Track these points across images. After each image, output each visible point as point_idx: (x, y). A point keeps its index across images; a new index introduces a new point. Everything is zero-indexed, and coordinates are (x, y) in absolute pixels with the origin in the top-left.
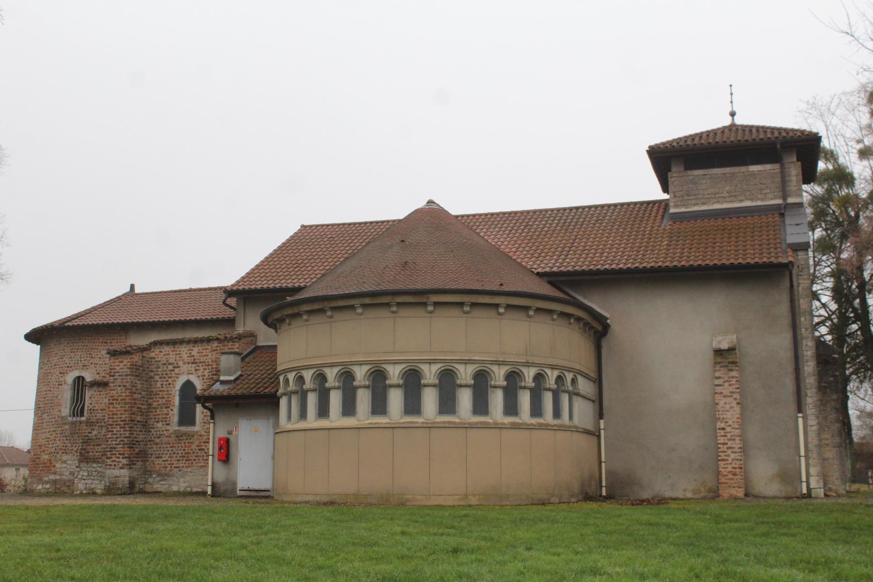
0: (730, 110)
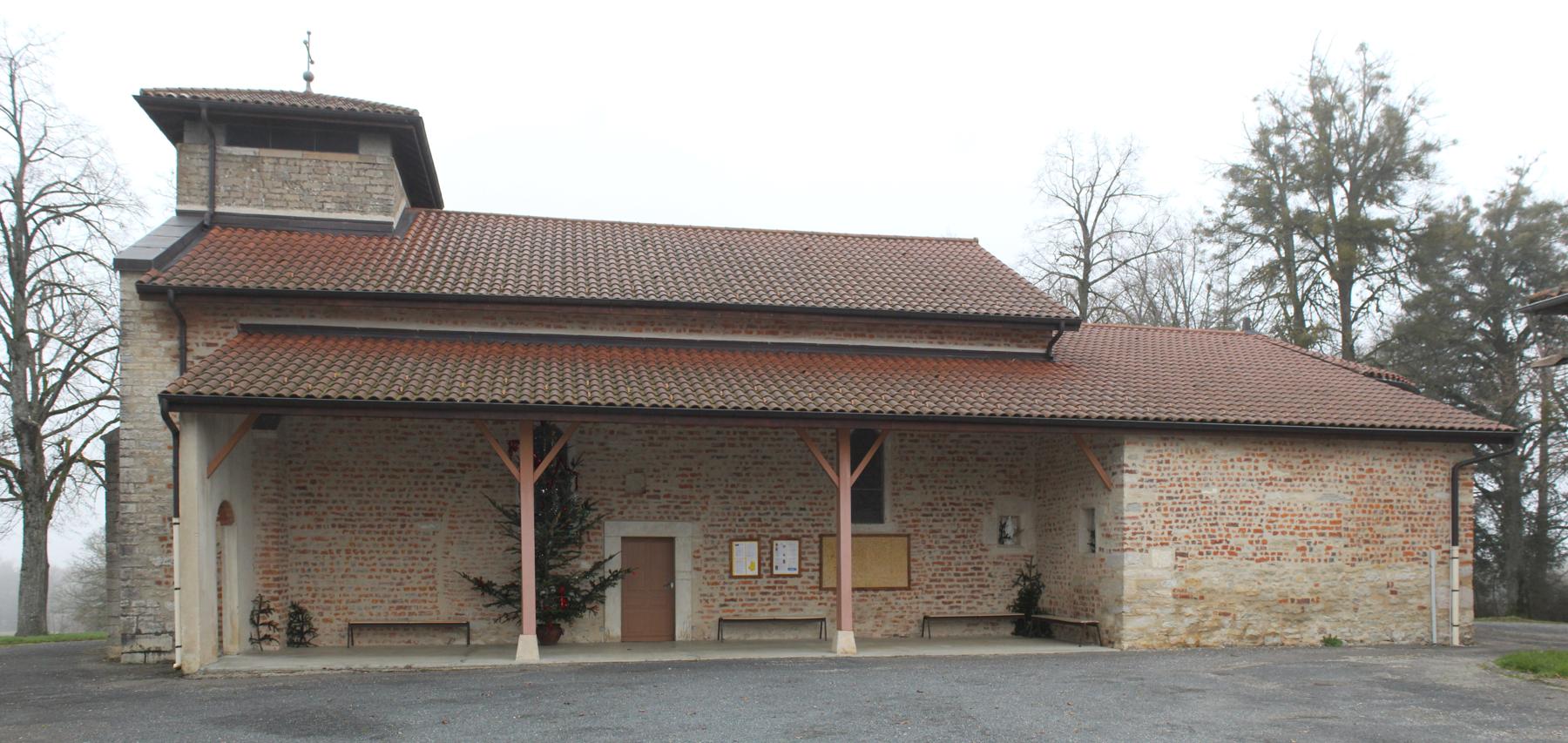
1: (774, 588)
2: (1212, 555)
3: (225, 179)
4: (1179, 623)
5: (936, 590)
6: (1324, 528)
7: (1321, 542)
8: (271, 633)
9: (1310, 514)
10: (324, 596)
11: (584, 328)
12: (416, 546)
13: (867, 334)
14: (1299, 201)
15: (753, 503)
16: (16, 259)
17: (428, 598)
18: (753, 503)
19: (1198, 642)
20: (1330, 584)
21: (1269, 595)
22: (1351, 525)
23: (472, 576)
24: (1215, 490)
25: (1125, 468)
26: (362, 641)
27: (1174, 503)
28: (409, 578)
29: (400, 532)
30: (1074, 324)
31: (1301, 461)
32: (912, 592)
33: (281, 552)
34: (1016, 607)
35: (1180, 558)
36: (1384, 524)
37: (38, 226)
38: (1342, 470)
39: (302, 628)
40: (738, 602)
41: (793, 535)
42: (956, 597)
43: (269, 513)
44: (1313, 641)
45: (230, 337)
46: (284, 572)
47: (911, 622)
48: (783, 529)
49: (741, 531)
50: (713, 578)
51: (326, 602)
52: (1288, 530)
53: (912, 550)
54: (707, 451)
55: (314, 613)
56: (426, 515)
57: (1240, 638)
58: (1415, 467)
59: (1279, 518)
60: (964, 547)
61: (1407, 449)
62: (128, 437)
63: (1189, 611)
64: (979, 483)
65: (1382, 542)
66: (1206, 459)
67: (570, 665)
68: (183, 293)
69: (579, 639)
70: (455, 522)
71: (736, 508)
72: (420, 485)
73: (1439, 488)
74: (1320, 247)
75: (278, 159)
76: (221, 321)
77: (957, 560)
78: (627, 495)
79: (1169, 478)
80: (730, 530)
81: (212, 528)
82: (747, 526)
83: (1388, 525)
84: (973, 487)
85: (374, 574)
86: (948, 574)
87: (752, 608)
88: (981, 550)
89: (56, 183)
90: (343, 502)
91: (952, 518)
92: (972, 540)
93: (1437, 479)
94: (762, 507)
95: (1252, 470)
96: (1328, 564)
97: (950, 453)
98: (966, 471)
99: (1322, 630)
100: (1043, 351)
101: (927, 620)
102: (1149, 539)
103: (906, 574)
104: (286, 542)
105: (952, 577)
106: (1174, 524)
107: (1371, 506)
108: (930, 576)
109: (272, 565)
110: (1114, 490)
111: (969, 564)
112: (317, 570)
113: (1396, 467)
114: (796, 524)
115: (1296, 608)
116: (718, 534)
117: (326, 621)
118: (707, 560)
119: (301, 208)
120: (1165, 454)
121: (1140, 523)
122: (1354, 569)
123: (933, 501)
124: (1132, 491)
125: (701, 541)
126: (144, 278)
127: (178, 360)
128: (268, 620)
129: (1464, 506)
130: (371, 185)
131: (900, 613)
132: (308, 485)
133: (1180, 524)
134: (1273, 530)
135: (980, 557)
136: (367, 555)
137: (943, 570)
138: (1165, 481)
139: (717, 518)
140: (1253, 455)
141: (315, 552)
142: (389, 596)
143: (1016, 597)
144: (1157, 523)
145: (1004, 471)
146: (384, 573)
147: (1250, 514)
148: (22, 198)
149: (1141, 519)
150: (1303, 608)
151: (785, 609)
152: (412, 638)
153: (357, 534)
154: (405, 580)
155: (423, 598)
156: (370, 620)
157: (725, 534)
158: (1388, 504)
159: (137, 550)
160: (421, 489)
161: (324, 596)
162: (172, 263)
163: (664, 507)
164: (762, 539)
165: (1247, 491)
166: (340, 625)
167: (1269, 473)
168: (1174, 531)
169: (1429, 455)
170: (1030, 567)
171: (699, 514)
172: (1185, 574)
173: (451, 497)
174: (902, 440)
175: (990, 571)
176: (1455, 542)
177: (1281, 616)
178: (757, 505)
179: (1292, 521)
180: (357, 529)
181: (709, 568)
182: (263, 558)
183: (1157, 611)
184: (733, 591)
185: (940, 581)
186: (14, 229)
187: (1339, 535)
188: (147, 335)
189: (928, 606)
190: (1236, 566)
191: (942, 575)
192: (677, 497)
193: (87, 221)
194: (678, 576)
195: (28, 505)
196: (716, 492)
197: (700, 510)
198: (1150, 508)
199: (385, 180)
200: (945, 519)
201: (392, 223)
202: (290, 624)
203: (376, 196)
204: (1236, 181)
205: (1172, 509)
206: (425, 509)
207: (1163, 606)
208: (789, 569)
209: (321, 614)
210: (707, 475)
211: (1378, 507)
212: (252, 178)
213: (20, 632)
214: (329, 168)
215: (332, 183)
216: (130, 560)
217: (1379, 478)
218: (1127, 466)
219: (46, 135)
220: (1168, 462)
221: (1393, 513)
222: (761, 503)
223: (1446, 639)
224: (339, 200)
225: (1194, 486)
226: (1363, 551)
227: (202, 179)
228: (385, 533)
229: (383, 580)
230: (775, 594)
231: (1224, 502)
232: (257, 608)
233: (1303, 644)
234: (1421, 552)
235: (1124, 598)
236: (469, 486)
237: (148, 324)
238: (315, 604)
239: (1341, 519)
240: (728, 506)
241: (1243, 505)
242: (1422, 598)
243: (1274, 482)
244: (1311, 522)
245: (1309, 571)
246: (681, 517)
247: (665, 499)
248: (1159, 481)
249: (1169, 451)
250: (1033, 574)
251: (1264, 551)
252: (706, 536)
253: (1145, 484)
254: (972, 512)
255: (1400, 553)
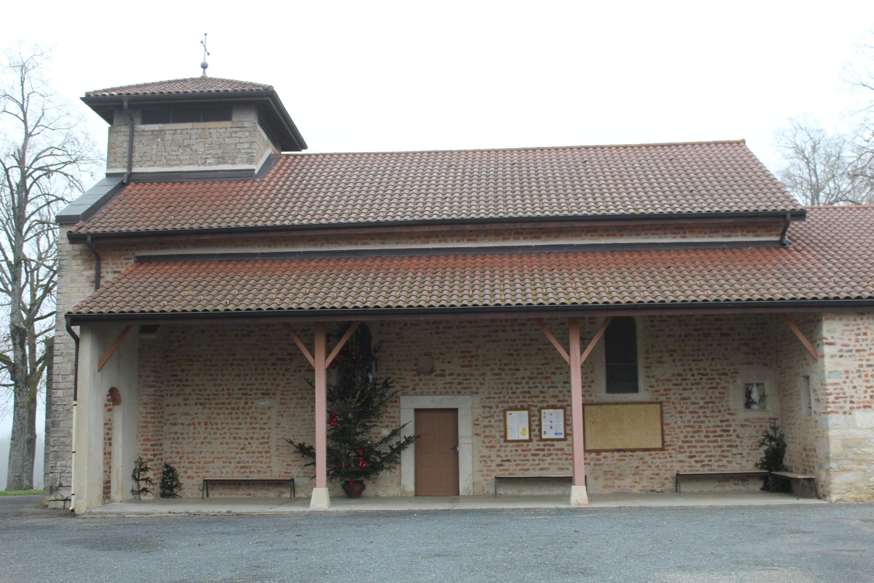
0: (202, 61)
1: (543, 450)
5: (688, 450)
8: (147, 486)
10: (188, 458)
12: (255, 418)
13: (618, 234)
15: (523, 378)
16: (18, 207)
17: (264, 460)
18: (523, 378)
23: (297, 442)
25: (825, 341)
26: (215, 494)
28: (250, 444)
30: (800, 215)
32: (666, 453)
33: (157, 424)
34: (763, 465)
37: (35, 181)
39: (172, 484)
40: (513, 463)
41: (559, 404)
46: (159, 439)
47: (666, 479)
49: (513, 402)
50: (490, 442)
51: (190, 463)
53: (665, 415)
54: (484, 337)
55: (180, 471)
56: (263, 394)
60: (712, 411)
62: (59, 342)
64: (724, 355)
67: (349, 512)
70: (285, 399)
71: (509, 383)
75: (176, 130)
76: (124, 255)
77: (707, 423)
81: (101, 409)
82: (518, 397)
85: (224, 441)
86: (699, 436)
88: (729, 414)
90: (203, 385)
91: (700, 387)
92: (720, 405)
94: (531, 382)
97: (696, 330)
98: (711, 345)
100: (777, 239)
101: (680, 478)
102: (852, 402)
103: (660, 437)
104: (162, 417)
105: (703, 438)
109: (150, 434)
110: (819, 360)
111: (718, 426)
112: (183, 438)
114: (561, 395)
116: (493, 405)
117: (189, 477)
118: (485, 427)
119: (190, 164)
120: (862, 327)
121: (842, 389)
123: (682, 372)
124: (833, 360)
125: (479, 411)
126: (73, 229)
127: (94, 284)
128: (146, 476)
131: (656, 471)
132: (179, 373)
135: (727, 421)
136: (219, 426)
137: (694, 432)
138: (864, 350)
139: (493, 391)
141: (183, 424)
143: (763, 455)
144: (858, 388)
145: (746, 344)
146: (232, 440)
148: (24, 165)
149: (843, 385)
152: (252, 492)
153: (213, 410)
154: (247, 446)
155: (261, 459)
156: (221, 477)
157: (500, 405)
159: (62, 424)
160: (260, 374)
161: (188, 458)
162: (94, 216)
163: (449, 383)
164: (532, 408)
170: (774, 429)
171: (477, 388)
173: (282, 380)
174: (651, 321)
175: (738, 432)
178: (527, 380)
180: (213, 406)
181: (487, 434)
182: (144, 429)
183: (864, 467)
184: (508, 453)
185: (691, 442)
188: (75, 268)
189: (681, 464)
192: (459, 375)
193: (66, 175)
194: (461, 441)
195: (17, 390)
196: (492, 370)
197: (478, 385)
198: (851, 375)
199: (249, 138)
200: (694, 387)
201: (254, 170)
202: (163, 480)
203: (243, 151)
206: (262, 390)
208: (556, 434)
209: (186, 472)
210: (484, 356)
213: (9, 488)
214: (210, 133)
215: (212, 144)
216: (57, 432)
218: (826, 339)
219: (43, 115)
220: (865, 334)
222: (530, 378)
224: (217, 156)
227: (124, 150)
228: (233, 409)
229: (231, 446)
230: (544, 455)
232: (138, 467)
235: (831, 455)
237: (76, 259)
238: (182, 465)
246: (463, 391)
247: (450, 377)
248: (857, 351)
249: (867, 325)
250: (778, 435)
252: (484, 407)
253: (844, 354)
254: (719, 381)
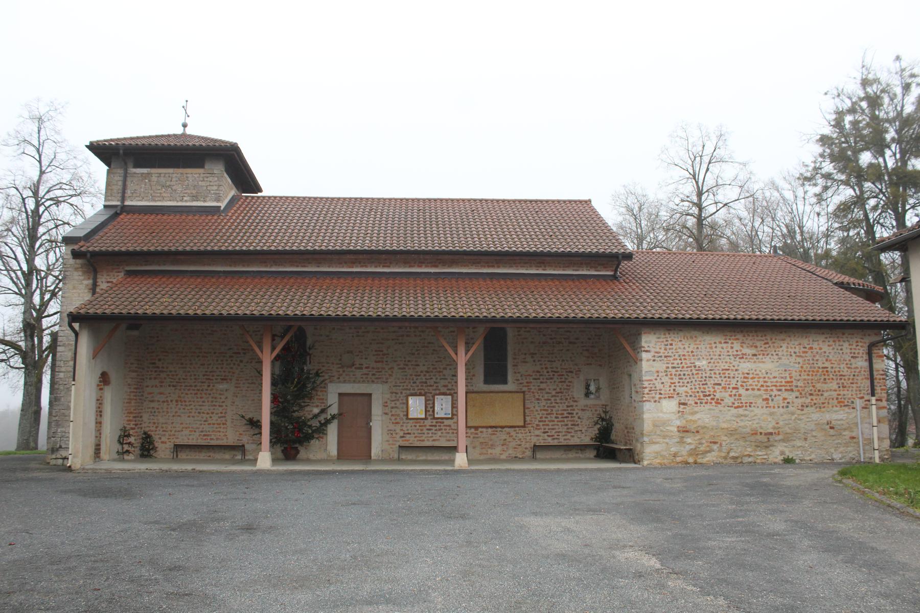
1: (436, 426)
2: (704, 404)
3: (131, 186)
4: (682, 449)
5: (542, 427)
6: (781, 386)
7: (779, 395)
8: (129, 449)
9: (771, 377)
10: (162, 427)
11: (318, 267)
12: (216, 398)
14: (866, 158)
15: (422, 372)
16: (32, 228)
17: (222, 430)
18: (422, 372)
19: (696, 460)
20: (786, 422)
21: (744, 430)
22: (799, 384)
23: (247, 417)
24: (704, 362)
25: (643, 349)
26: (183, 455)
27: (677, 371)
28: (211, 417)
29: (207, 390)
31: (763, 342)
32: (527, 429)
34: (597, 439)
35: (682, 406)
36: (823, 383)
38: (791, 348)
40: (412, 435)
41: (448, 392)
42: (556, 432)
43: (132, 378)
44: (776, 460)
45: (120, 277)
46: (140, 413)
47: (526, 448)
48: (441, 389)
49: (414, 390)
51: (163, 431)
52: (756, 388)
53: (526, 401)
54: (393, 340)
55: (156, 438)
56: (222, 379)
57: (725, 458)
58: (842, 345)
59: (749, 380)
60: (561, 399)
61: (836, 334)
63: (689, 440)
64: (571, 358)
65: (822, 395)
66: (698, 342)
67: (286, 471)
68: (95, 255)
69: (311, 456)
71: (411, 375)
72: (219, 362)
73: (859, 359)
74: (879, 189)
75: (160, 174)
77: (557, 408)
78: (342, 367)
79: (673, 355)
80: (407, 389)
82: (418, 386)
83: (826, 383)
84: (567, 361)
87: (421, 439)
89: (58, 184)
90: (175, 371)
93: (858, 353)
94: (427, 374)
95: (729, 349)
96: (785, 410)
97: (551, 339)
98: (562, 350)
99: (782, 453)
100: (612, 273)
101: (536, 448)
102: (660, 394)
104: (142, 395)
105: (554, 419)
106: (677, 384)
107: (813, 371)
108: (539, 418)
110: (639, 363)
112: (159, 412)
113: (829, 346)
115: (764, 438)
117: (162, 442)
118: (392, 408)
119: (170, 200)
120: (669, 339)
122: (803, 412)
125: (388, 396)
128: (128, 441)
129: (878, 371)
130: (210, 185)
131: (519, 443)
132: (157, 361)
133: (681, 384)
134: (745, 388)
135: (572, 406)
136: (187, 403)
138: (670, 357)
139: (398, 381)
140: (730, 339)
141: (159, 401)
142: (198, 428)
145: (587, 350)
147: (729, 377)
149: (655, 382)
150: (768, 438)
151: (443, 439)
153: (182, 391)
155: (218, 429)
157: (404, 392)
158: (825, 370)
161: (162, 427)
163: (366, 374)
165: (726, 362)
166: (170, 445)
167: (741, 351)
168: (677, 389)
169: (851, 338)
170: (605, 412)
171: (387, 379)
172: (685, 416)
173: (237, 369)
174: (519, 331)
175: (579, 415)
176: (873, 394)
177: (753, 444)
178: (424, 373)
179: (758, 381)
181: (393, 413)
182: (128, 404)
184: (409, 428)
186: (32, 211)
187: (792, 390)
188: (77, 277)
189: (538, 438)
190: (721, 411)
191: (546, 418)
192: (373, 368)
194: (373, 418)
198: (660, 374)
201: (220, 207)
202: (142, 444)
203: (212, 192)
204: (823, 145)
205: (675, 375)
206: (222, 376)
207: (671, 437)
209: (160, 438)
210: (393, 355)
211: (818, 371)
212: (145, 185)
214: (187, 177)
217: (817, 353)
218: (644, 347)
219: (55, 157)
220: (671, 345)
221: (828, 375)
222: (427, 372)
223: (871, 458)
225: (690, 359)
226: (808, 400)
228: (198, 390)
230: (436, 430)
231: (711, 370)
232: (123, 434)
233: (769, 462)
234: (850, 401)
235: (644, 432)
236: (248, 362)
238: (157, 433)
239: (793, 380)
240: (406, 373)
241: (724, 372)
242: (853, 431)
243: (745, 357)
244: (772, 382)
245: (771, 414)
246: (376, 381)
248: (666, 357)
249: (673, 338)
250: (608, 417)
251: (740, 401)
253: (656, 359)
254: (566, 377)
255: (835, 401)
